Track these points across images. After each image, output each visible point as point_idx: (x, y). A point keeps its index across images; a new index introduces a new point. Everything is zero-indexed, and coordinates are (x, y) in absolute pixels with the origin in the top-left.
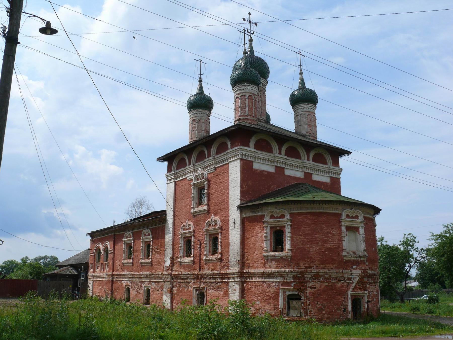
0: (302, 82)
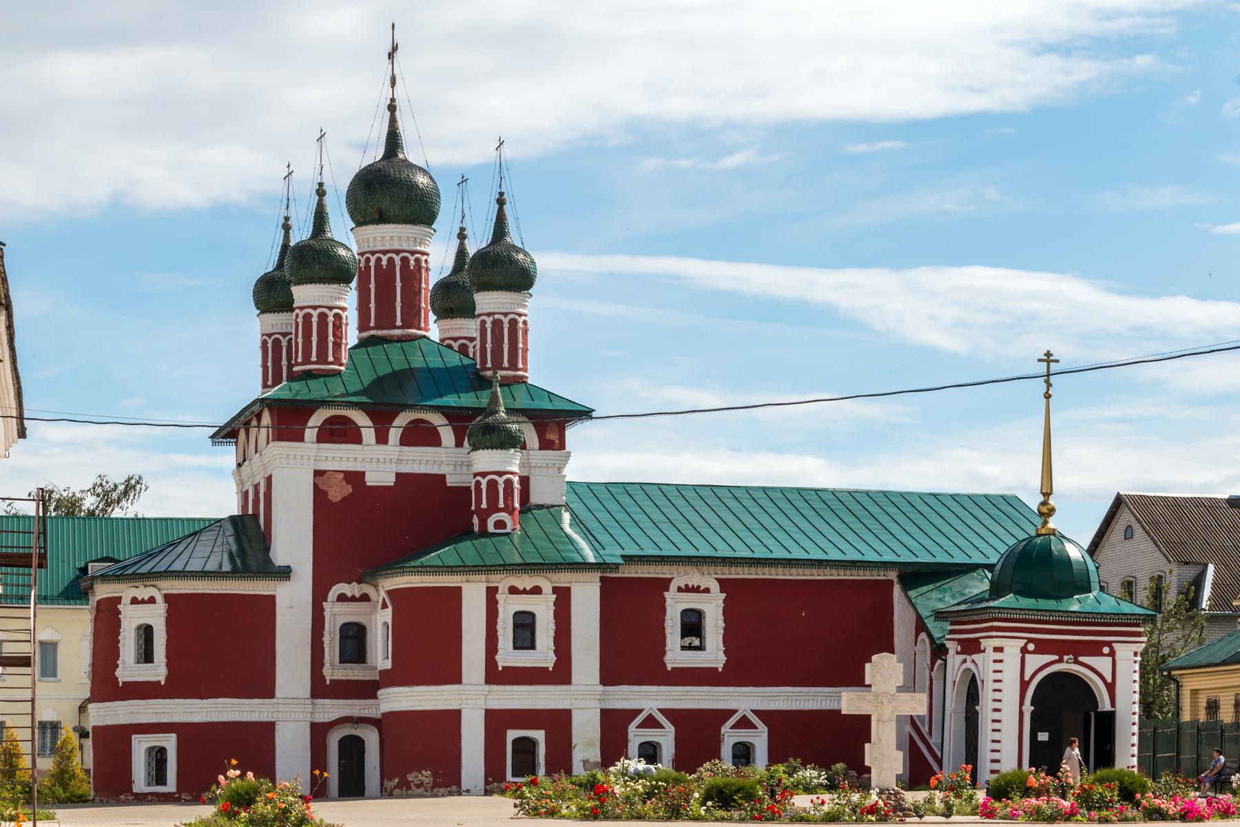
0: (393, 141)
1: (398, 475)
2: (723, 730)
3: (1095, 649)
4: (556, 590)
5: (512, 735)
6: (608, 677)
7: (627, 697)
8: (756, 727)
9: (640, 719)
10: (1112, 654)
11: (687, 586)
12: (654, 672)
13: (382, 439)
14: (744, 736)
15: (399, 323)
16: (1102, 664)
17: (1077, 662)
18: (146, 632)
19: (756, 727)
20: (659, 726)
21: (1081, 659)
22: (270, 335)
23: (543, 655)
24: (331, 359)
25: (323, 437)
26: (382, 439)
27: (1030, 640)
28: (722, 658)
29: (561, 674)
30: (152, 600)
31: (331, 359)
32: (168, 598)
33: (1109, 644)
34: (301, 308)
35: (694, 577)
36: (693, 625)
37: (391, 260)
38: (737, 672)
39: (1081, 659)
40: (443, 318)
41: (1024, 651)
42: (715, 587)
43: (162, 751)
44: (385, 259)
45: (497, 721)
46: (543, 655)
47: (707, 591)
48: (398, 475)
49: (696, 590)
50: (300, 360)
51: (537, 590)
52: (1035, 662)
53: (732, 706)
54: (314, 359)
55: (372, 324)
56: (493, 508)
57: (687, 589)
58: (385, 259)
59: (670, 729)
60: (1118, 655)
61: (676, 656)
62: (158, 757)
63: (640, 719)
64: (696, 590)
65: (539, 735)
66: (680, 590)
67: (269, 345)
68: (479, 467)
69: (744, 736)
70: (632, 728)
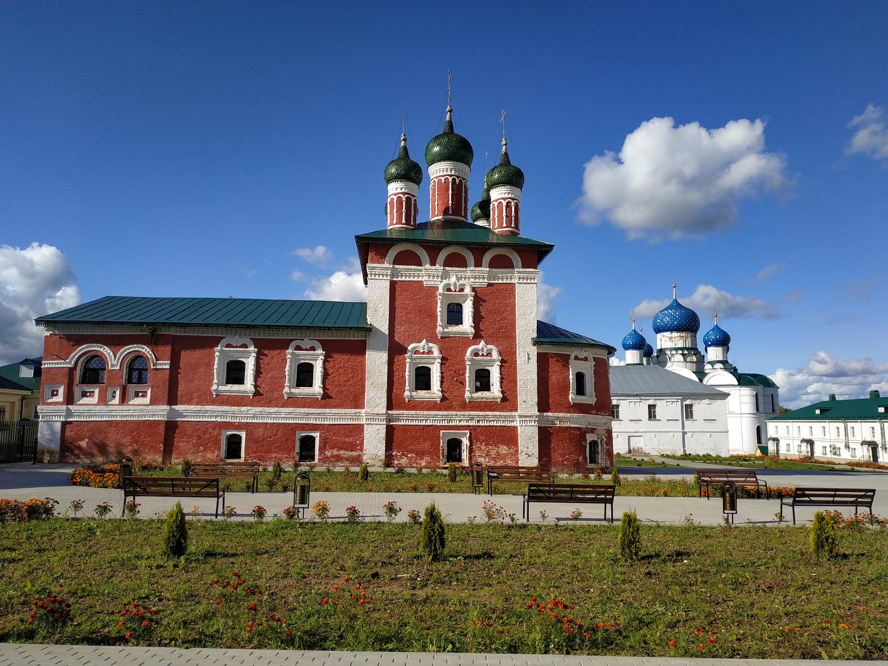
18: (580, 377)
30: (586, 359)
32: (595, 359)
34: (496, 201)
46: (589, 398)
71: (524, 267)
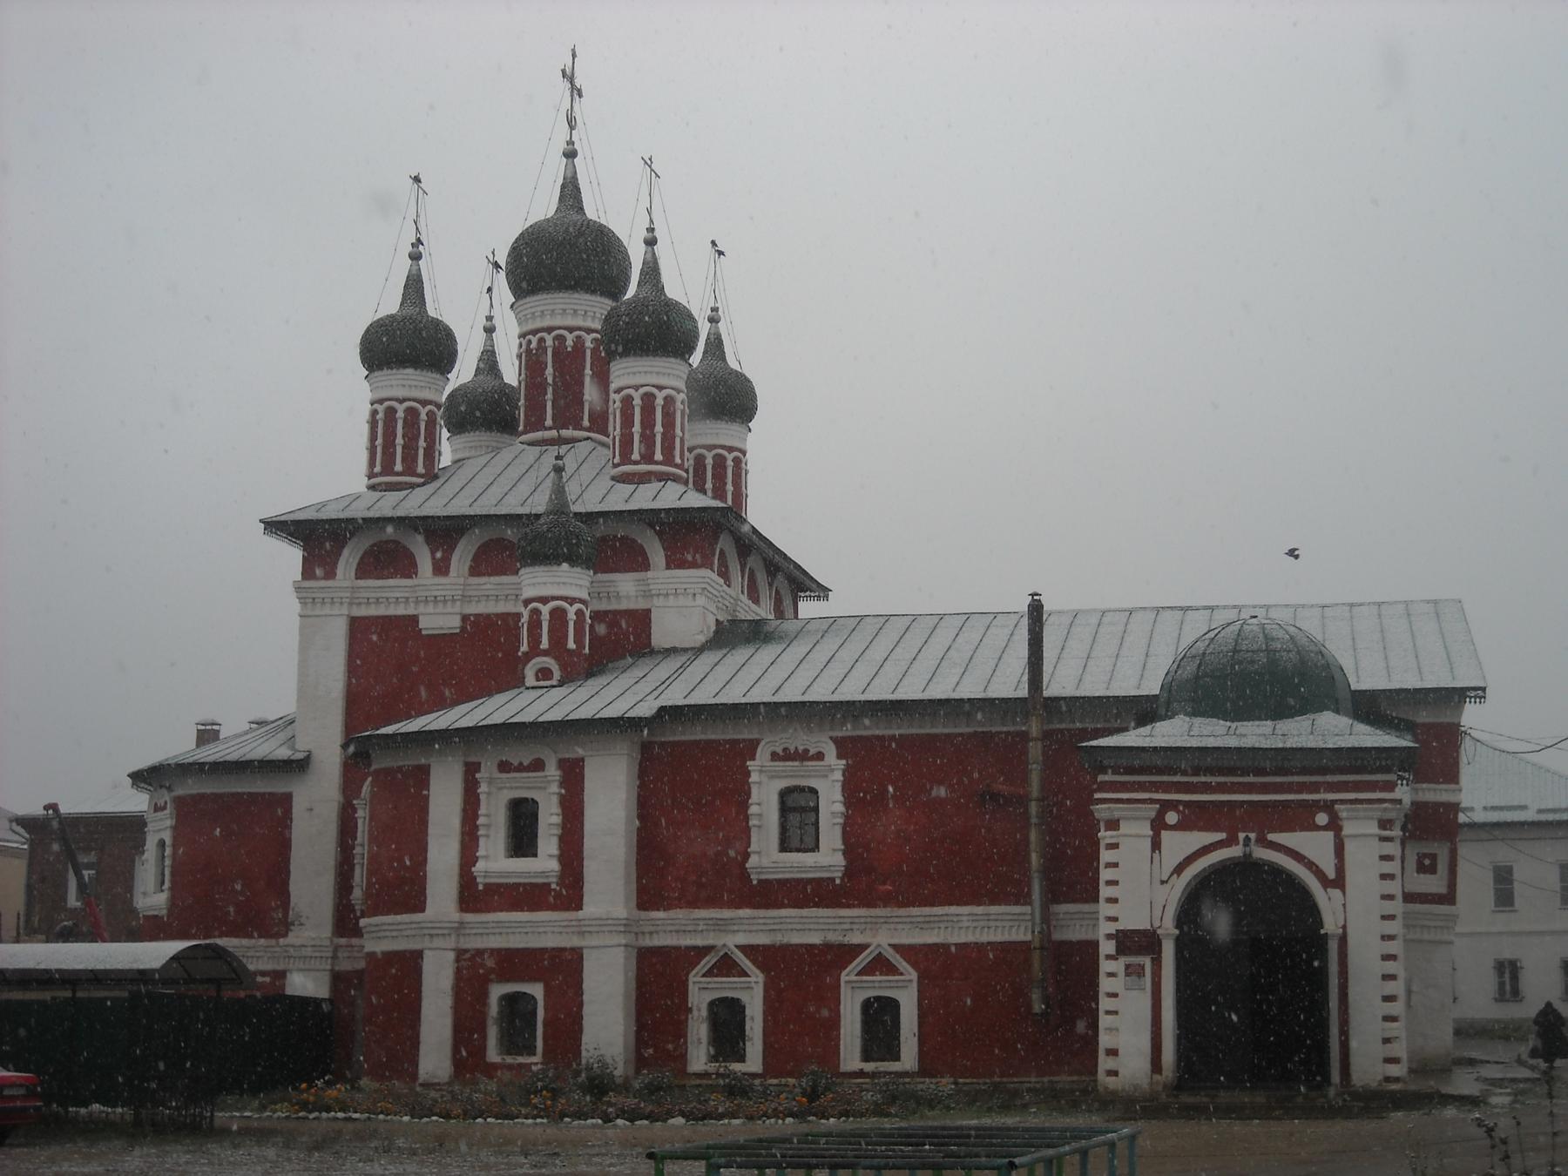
1: (465, 618)
2: (692, 979)
3: (1299, 817)
4: (562, 764)
5: (497, 991)
6: (650, 894)
7: (676, 928)
8: (745, 974)
9: (708, 961)
10: (1334, 825)
11: (785, 750)
12: (737, 887)
13: (441, 568)
14: (726, 987)
15: (549, 422)
16: (1315, 845)
17: (1263, 842)
18: (162, 844)
19: (745, 974)
20: (890, 969)
21: (1271, 837)
22: (381, 401)
23: (545, 863)
24: (658, 456)
25: (363, 571)
26: (441, 568)
27: (1166, 806)
28: (839, 860)
29: (568, 891)
31: (658, 456)
33: (1328, 807)
34: (618, 391)
35: (799, 739)
36: (797, 809)
37: (579, 342)
38: (860, 884)
39: (1271, 837)
40: (380, 368)
41: (1158, 825)
42: (830, 751)
43: (891, 1006)
44: (570, 339)
45: (473, 975)
46: (545, 863)
47: (820, 756)
48: (465, 618)
49: (803, 756)
50: (636, 456)
51: (538, 765)
52: (1179, 844)
53: (856, 939)
54: (398, 467)
55: (549, 422)
56: (535, 651)
57: (788, 756)
58: (570, 339)
59: (757, 978)
60: (1348, 829)
61: (767, 856)
62: (880, 1015)
63: (708, 961)
64: (803, 756)
65: (536, 990)
66: (775, 756)
67: (380, 416)
68: (529, 593)
69: (726, 987)
70: (695, 979)
71: (674, 562)
